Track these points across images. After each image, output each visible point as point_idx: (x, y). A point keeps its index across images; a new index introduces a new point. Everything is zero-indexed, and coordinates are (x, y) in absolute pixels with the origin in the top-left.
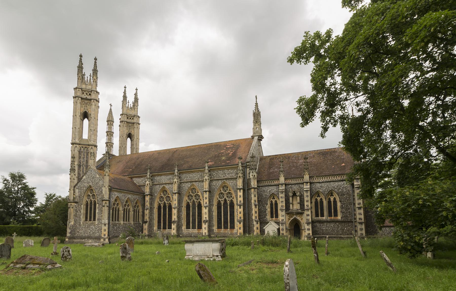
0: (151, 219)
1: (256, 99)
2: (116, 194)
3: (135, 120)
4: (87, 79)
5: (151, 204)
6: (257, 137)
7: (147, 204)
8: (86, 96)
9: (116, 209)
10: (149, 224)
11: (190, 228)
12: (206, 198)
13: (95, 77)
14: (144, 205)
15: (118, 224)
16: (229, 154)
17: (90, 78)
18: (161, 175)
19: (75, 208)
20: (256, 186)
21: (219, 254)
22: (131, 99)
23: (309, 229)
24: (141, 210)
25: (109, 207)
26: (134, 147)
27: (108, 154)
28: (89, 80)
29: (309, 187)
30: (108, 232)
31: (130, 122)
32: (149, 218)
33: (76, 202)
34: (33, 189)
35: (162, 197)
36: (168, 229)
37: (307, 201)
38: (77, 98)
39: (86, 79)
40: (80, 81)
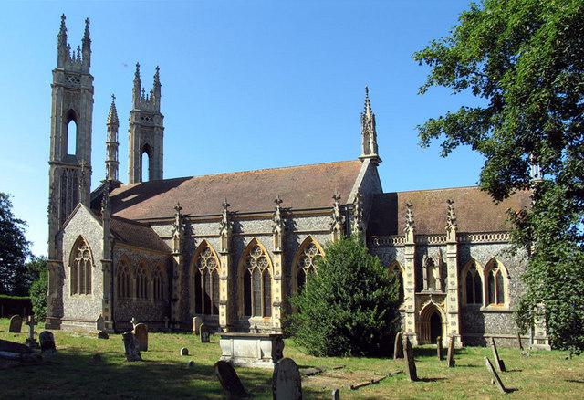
12: (277, 264)
21: (221, 281)
22: (148, 86)
23: (453, 324)
27: (112, 184)
29: (455, 251)
30: (112, 314)
34: (20, 221)
37: (452, 276)
39: (72, 54)
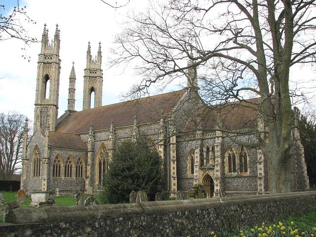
0: (93, 175)
2: (57, 152)
3: (98, 74)
5: (93, 160)
7: (89, 160)
8: (48, 60)
14: (86, 161)
18: (101, 132)
20: (175, 142)
22: (94, 54)
24: (84, 166)
25: (49, 163)
26: (98, 100)
27: (70, 112)
31: (94, 76)
32: (91, 173)
33: (28, 160)
40: (44, 47)
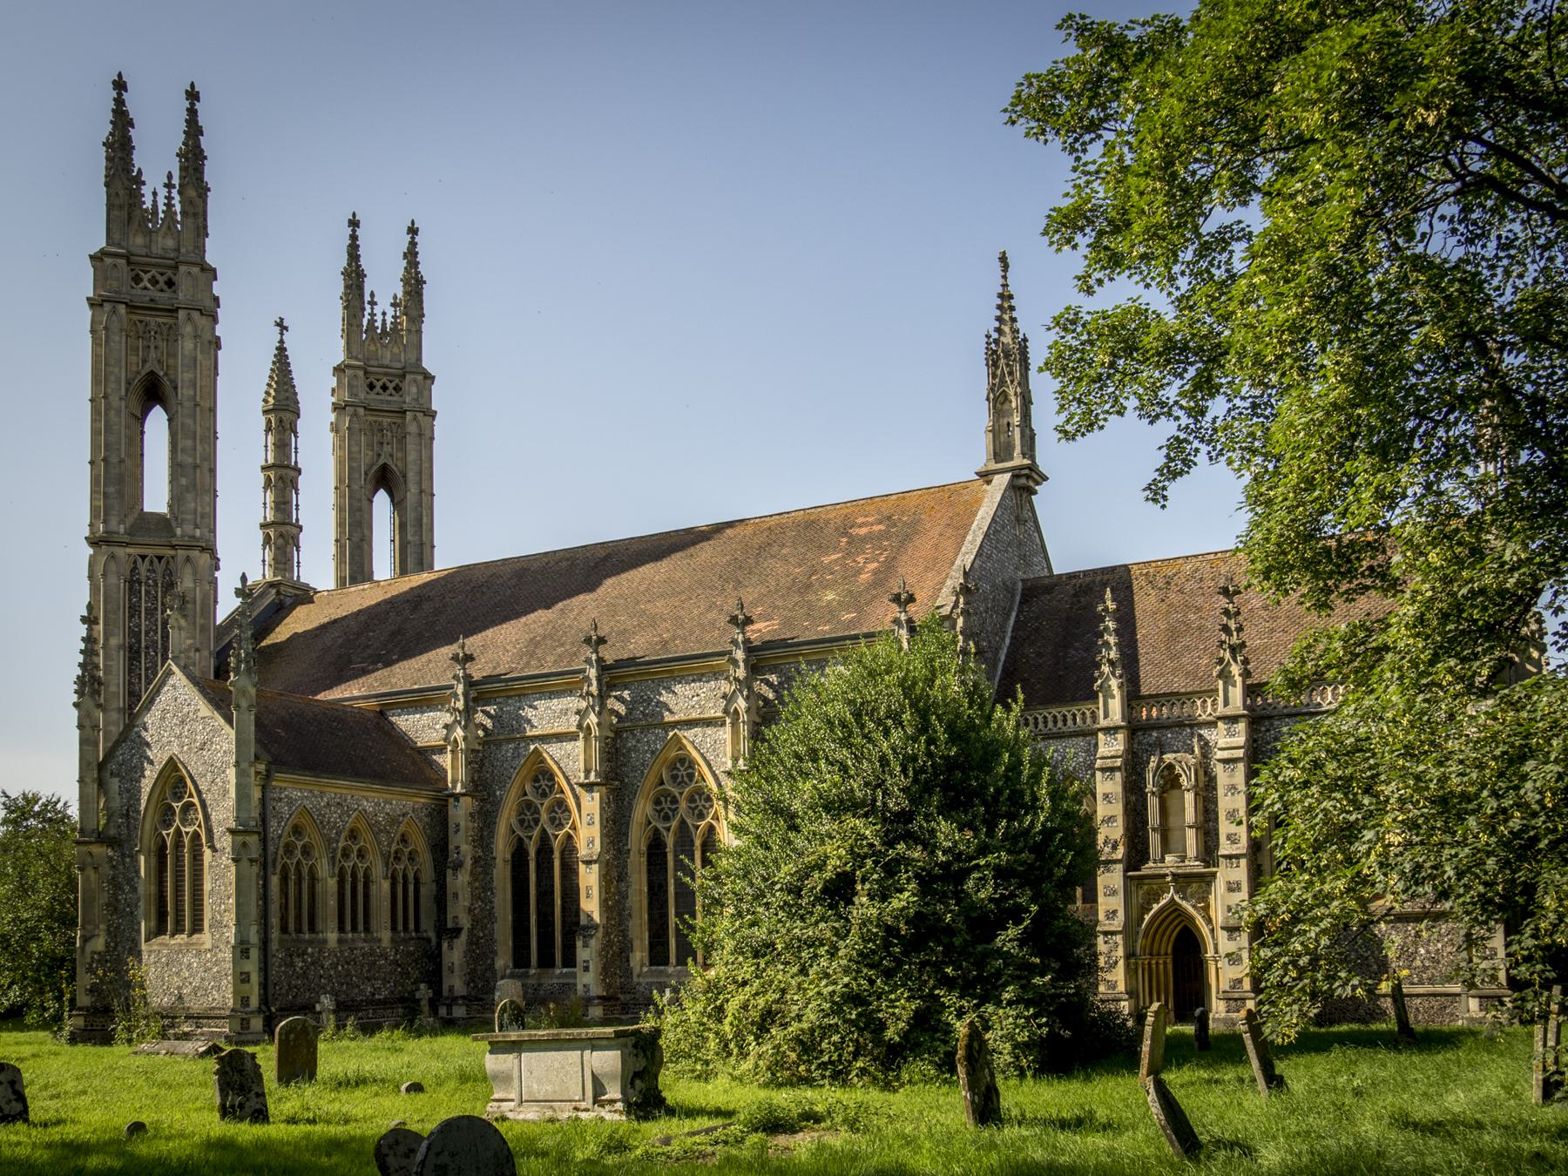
1: (1006, 267)
4: (155, 202)
6: (1008, 476)
8: (153, 292)
9: (405, 877)
10: (470, 943)
11: (666, 963)
13: (192, 193)
15: (310, 942)
16: (859, 572)
17: (169, 198)
19: (106, 870)
22: (384, 285)
28: (161, 208)
30: (264, 985)
35: (529, 805)
36: (564, 965)
38: (107, 307)
39: (148, 204)
